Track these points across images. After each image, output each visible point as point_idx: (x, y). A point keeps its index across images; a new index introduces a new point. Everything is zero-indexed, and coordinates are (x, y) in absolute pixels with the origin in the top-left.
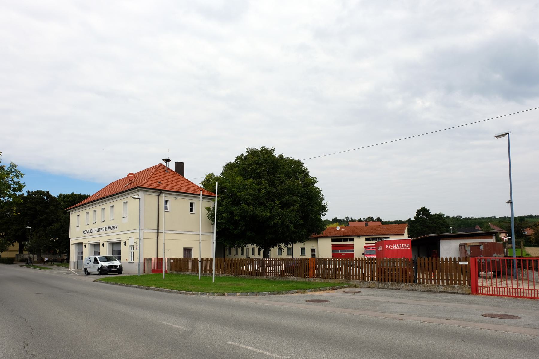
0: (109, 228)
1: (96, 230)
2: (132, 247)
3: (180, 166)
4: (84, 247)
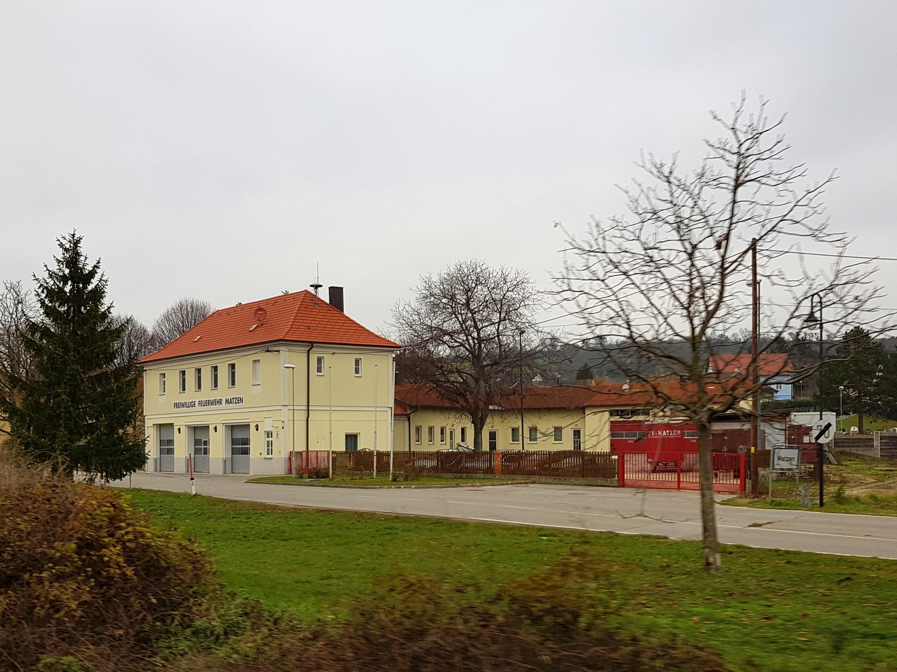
0: (227, 401)
1: (200, 403)
2: (269, 434)
3: (336, 293)
4: (176, 431)
